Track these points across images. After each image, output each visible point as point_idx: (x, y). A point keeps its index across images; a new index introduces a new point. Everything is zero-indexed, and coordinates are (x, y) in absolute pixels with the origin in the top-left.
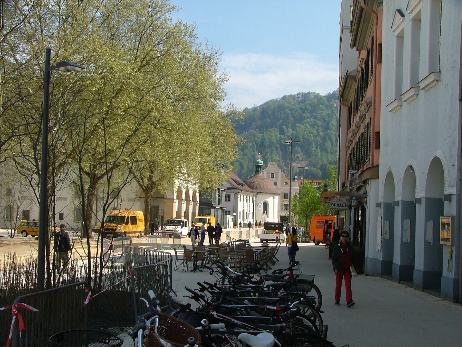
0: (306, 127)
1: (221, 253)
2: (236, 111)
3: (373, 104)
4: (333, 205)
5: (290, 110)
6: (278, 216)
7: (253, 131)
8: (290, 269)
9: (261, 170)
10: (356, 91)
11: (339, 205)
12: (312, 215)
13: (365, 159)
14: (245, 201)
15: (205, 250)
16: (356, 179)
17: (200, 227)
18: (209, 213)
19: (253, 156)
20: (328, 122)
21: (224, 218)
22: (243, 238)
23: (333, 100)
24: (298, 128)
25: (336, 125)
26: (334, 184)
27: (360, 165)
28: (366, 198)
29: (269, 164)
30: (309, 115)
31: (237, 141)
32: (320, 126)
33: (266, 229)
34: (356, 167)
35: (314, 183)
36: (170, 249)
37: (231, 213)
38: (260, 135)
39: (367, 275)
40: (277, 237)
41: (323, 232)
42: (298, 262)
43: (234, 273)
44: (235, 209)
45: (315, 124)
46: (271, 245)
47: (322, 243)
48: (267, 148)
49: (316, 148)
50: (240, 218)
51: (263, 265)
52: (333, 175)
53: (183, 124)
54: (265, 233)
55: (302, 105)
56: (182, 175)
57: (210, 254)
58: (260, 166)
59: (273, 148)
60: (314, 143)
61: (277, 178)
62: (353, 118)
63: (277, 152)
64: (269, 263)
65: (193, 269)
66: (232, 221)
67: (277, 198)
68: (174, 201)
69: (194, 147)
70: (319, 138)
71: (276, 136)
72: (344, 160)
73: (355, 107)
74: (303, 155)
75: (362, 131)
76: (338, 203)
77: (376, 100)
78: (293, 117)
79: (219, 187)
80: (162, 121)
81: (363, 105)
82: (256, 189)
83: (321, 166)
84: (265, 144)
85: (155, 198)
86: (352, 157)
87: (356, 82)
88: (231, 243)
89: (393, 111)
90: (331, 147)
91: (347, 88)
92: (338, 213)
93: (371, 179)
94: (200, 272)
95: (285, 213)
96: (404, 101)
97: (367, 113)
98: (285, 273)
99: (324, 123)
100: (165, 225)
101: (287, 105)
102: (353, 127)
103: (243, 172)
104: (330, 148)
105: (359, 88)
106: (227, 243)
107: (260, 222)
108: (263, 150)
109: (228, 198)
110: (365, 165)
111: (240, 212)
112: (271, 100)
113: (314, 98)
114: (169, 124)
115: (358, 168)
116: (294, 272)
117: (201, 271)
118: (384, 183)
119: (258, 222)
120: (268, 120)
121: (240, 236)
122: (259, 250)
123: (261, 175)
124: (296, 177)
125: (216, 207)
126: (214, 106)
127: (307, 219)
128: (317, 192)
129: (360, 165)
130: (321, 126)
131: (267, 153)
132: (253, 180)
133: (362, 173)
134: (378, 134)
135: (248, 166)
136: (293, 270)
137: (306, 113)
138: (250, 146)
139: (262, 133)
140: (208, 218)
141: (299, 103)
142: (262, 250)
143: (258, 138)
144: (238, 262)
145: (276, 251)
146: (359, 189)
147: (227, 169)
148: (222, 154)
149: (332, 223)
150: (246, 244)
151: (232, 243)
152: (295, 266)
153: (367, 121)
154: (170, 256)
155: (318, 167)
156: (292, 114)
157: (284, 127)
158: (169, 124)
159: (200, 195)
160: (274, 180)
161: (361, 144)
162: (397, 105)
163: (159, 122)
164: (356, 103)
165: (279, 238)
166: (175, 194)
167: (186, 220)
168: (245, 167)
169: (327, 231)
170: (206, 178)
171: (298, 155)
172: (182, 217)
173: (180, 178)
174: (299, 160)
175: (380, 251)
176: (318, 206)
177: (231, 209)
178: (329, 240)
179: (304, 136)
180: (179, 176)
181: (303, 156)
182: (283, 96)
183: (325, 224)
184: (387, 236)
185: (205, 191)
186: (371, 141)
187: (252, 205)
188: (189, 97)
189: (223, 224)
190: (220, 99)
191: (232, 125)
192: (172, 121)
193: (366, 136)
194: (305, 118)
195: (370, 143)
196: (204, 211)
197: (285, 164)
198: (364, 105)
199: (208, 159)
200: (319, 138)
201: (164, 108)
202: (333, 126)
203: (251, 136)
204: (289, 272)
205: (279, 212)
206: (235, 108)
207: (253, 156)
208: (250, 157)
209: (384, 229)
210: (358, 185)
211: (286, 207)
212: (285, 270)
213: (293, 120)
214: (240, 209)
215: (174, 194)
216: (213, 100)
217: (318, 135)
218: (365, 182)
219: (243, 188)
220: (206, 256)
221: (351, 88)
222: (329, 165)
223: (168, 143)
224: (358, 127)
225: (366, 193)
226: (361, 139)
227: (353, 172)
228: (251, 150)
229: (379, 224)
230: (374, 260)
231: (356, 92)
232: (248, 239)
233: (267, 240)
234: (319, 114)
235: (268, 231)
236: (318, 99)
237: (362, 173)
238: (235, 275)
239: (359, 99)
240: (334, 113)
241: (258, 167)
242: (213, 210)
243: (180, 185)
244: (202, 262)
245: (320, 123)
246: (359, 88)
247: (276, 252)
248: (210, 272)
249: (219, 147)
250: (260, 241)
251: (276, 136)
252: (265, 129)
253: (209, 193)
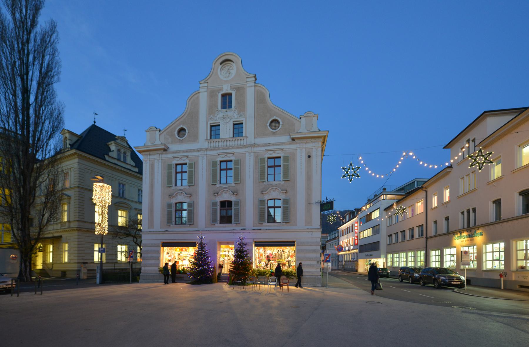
160: (233, 115)
205: (129, 283)
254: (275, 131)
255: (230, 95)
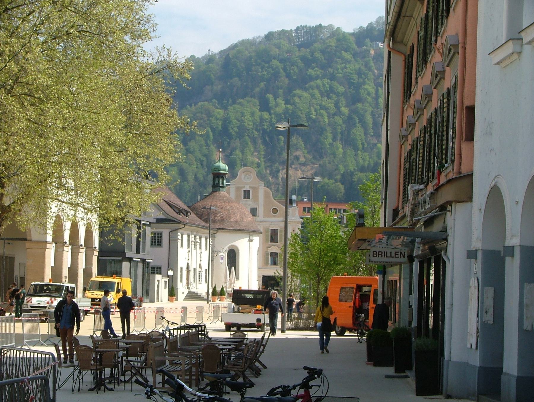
0: (313, 96)
1: (151, 351)
2: (175, 62)
3: (460, 50)
4: (375, 254)
5: (281, 61)
6: (259, 276)
7: (206, 103)
8: (305, 385)
9: (223, 184)
10: (423, 22)
11: (389, 255)
12: (330, 275)
13: (444, 161)
14: (192, 246)
15: (118, 347)
16: (424, 201)
17: (100, 299)
18: (119, 270)
19: (205, 155)
20: (358, 87)
21: (148, 280)
22: (191, 321)
23: (368, 41)
24: (297, 100)
25: (374, 92)
26: (373, 212)
27: (431, 174)
28: (446, 239)
29: (241, 172)
30: (318, 72)
31: (176, 124)
32: (342, 94)
33: (236, 303)
34: (422, 178)
35: (331, 209)
36: (42, 345)
37: (163, 270)
38: (220, 113)
39: (449, 397)
40: (259, 320)
41: (352, 308)
42: (321, 370)
43: (195, 395)
44: (172, 262)
45: (332, 90)
46: (251, 335)
47: (350, 333)
48: (234, 138)
49: (334, 139)
50: (181, 281)
51: (237, 376)
52: (372, 194)
53: (66, 88)
54: (235, 312)
55: (305, 52)
56: (64, 192)
57: (127, 355)
58: (222, 176)
59: (247, 138)
60: (329, 129)
61: (256, 200)
62: (416, 79)
63: (255, 148)
64: (248, 373)
65: (93, 386)
66: (165, 287)
67: (256, 240)
68: (48, 246)
69: (91, 136)
70: (339, 120)
71: (253, 114)
72: (397, 164)
73: (421, 56)
74: (308, 153)
75: (435, 103)
76: (386, 250)
77: (468, 42)
78: (288, 76)
79: (140, 218)
80: (24, 80)
81: (439, 52)
82: (214, 221)
83: (343, 175)
84: (231, 131)
85: (7, 239)
86: (414, 157)
87: (423, 4)
88: (168, 333)
89: (503, 64)
90: (363, 137)
91: (404, 17)
92: (383, 271)
93: (457, 202)
94: (107, 392)
95: (271, 271)
96: (526, 44)
97: (448, 69)
98: (294, 393)
99: (350, 88)
100: (28, 295)
101: (275, 51)
102: (417, 95)
103: (187, 186)
104: (361, 140)
105: (430, 17)
106: (161, 332)
107: (223, 288)
108: (226, 143)
109: (157, 241)
110: (443, 174)
111: (181, 268)
112: (243, 41)
113: (330, 37)
114: (37, 87)
115: (428, 178)
116: (312, 391)
117: (111, 390)
118: (483, 211)
119: (219, 289)
120: (236, 81)
121: (183, 319)
122: (228, 347)
123: (223, 192)
124: (294, 197)
125: (132, 258)
126: (129, 52)
127: (319, 283)
128: (338, 229)
129: (431, 174)
130: (344, 94)
131: (234, 149)
132: (208, 203)
133: (438, 188)
134: (471, 110)
135: (196, 175)
136: (311, 387)
137: (313, 69)
138: (201, 136)
139: (225, 108)
140: (116, 280)
141: (300, 46)
142: (233, 346)
143: (217, 119)
144: (186, 371)
145: (262, 347)
146: (429, 222)
147: (158, 181)
148: (148, 150)
149: (370, 292)
150: (199, 334)
151: (172, 331)
152: (315, 378)
153: (448, 83)
154: (51, 360)
155: (338, 177)
156: (285, 69)
157: (270, 96)
158: (37, 87)
159: (101, 235)
160: (250, 203)
161: (433, 131)
162: (511, 51)
163: (16, 81)
164: (422, 48)
165: (262, 322)
166: (50, 232)
167: (73, 285)
168: (191, 178)
169: (361, 307)
170: (114, 200)
171: (298, 153)
172: (64, 280)
173: (60, 198)
174: (300, 164)
175: (474, 347)
176: (342, 256)
177: (162, 262)
178: (366, 326)
179: (308, 115)
180: (58, 195)
181: (307, 156)
182: (266, 33)
183: (356, 294)
184: (489, 318)
185: (112, 226)
186: (457, 126)
187: (205, 254)
188: (79, 32)
189: (148, 294)
190: (144, 36)
191: (167, 91)
192: (43, 80)
193: (445, 115)
194: (311, 78)
195: (453, 128)
196: (109, 266)
197: (271, 171)
198: (441, 51)
199: (119, 160)
200: (339, 120)
201: (27, 53)
202: (369, 94)
203: (202, 113)
204: (302, 392)
205: (259, 268)
206: (172, 55)
207: (205, 155)
208: (199, 156)
209: (482, 303)
210: (429, 215)
211: (273, 259)
212: (294, 387)
213: (287, 81)
214: (182, 263)
215: (48, 231)
216: (127, 38)
217: (339, 112)
218: (443, 208)
219: (187, 220)
220: (120, 359)
221: (411, 16)
222: (361, 175)
223: (36, 125)
224: (428, 97)
225: (445, 230)
226: (433, 120)
227: (417, 187)
228: (203, 142)
229: (473, 293)
230: (464, 366)
231: (423, 26)
232: (199, 322)
233: (238, 326)
234: (340, 71)
235: (242, 306)
236: (338, 40)
237: (437, 190)
238: (196, 398)
239: (429, 40)
240: (370, 69)
241: (218, 177)
242: (126, 265)
243: (60, 214)
244: (112, 371)
245: (341, 89)
246: (430, 17)
247: (261, 350)
248: (146, 393)
249: (140, 135)
250: (224, 327)
251: (253, 114)
252: (230, 101)
253: (121, 230)
254: (275, 215)
255: (249, 191)
